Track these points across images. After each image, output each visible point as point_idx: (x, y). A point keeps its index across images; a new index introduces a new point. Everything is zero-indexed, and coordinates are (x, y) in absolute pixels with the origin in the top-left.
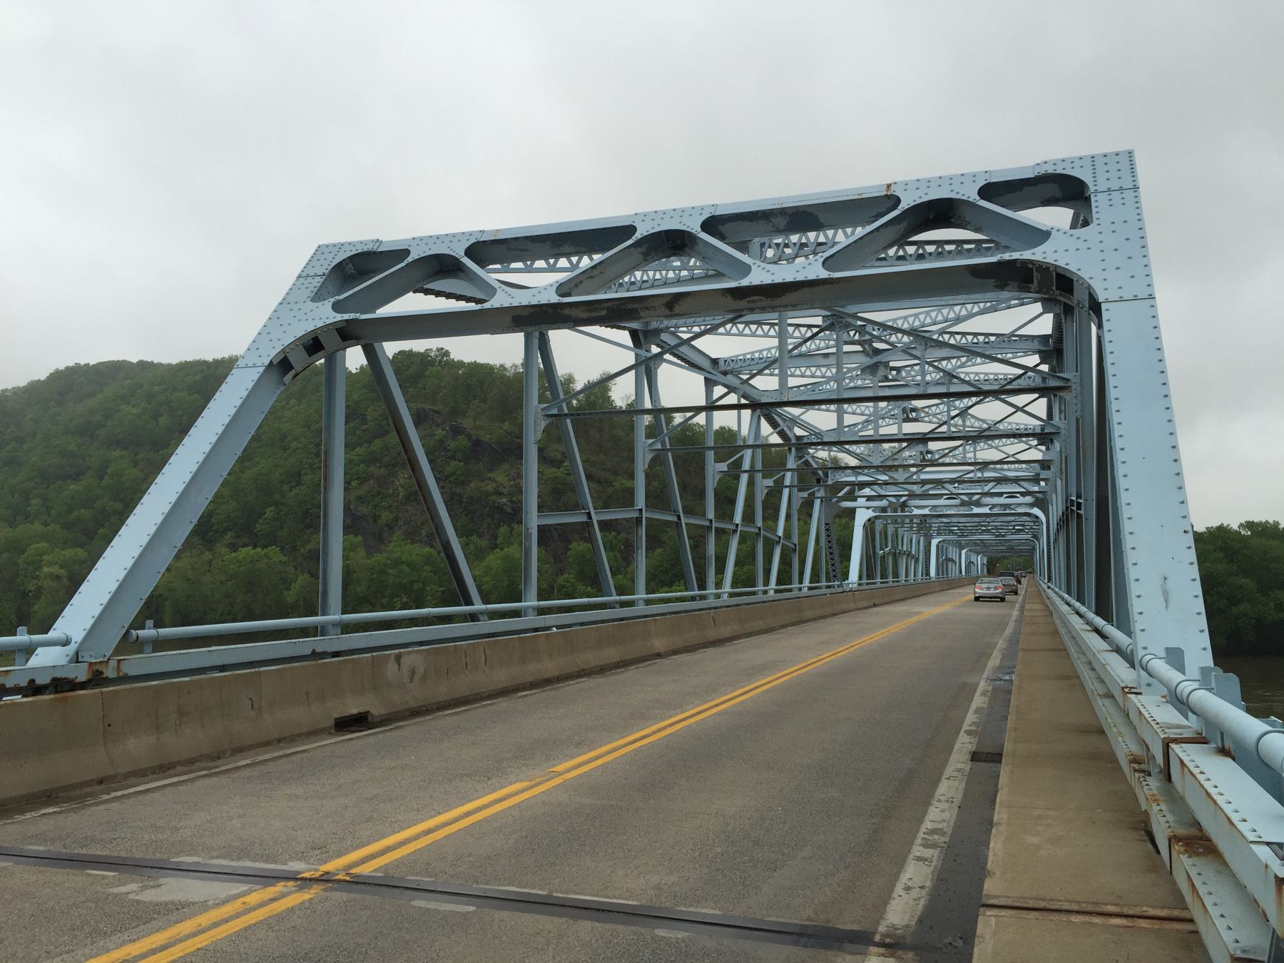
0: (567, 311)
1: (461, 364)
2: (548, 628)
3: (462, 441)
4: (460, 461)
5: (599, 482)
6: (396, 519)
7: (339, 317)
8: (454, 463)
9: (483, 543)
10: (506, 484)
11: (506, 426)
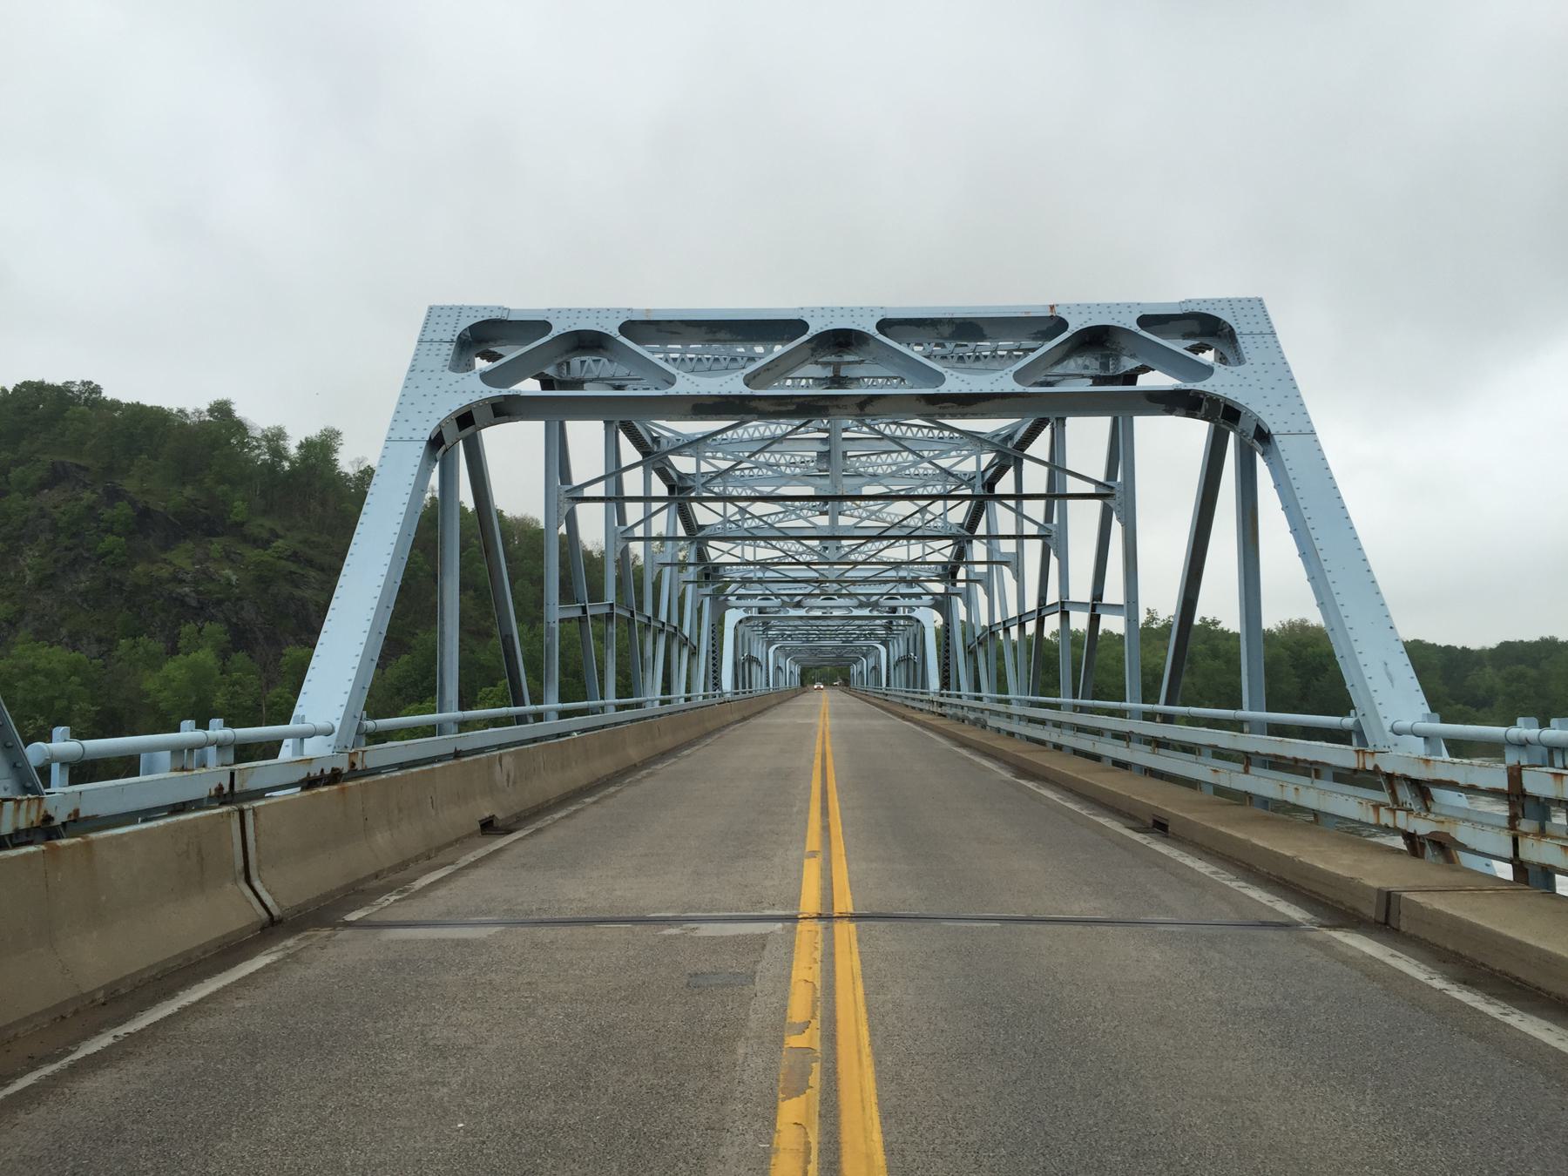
0: (753, 404)
1: (116, 405)
2: (568, 734)
3: (123, 509)
4: (119, 535)
5: (323, 570)
6: (22, 612)
7: (495, 392)
8: (110, 539)
9: (157, 646)
10: (189, 568)
11: (189, 491)
